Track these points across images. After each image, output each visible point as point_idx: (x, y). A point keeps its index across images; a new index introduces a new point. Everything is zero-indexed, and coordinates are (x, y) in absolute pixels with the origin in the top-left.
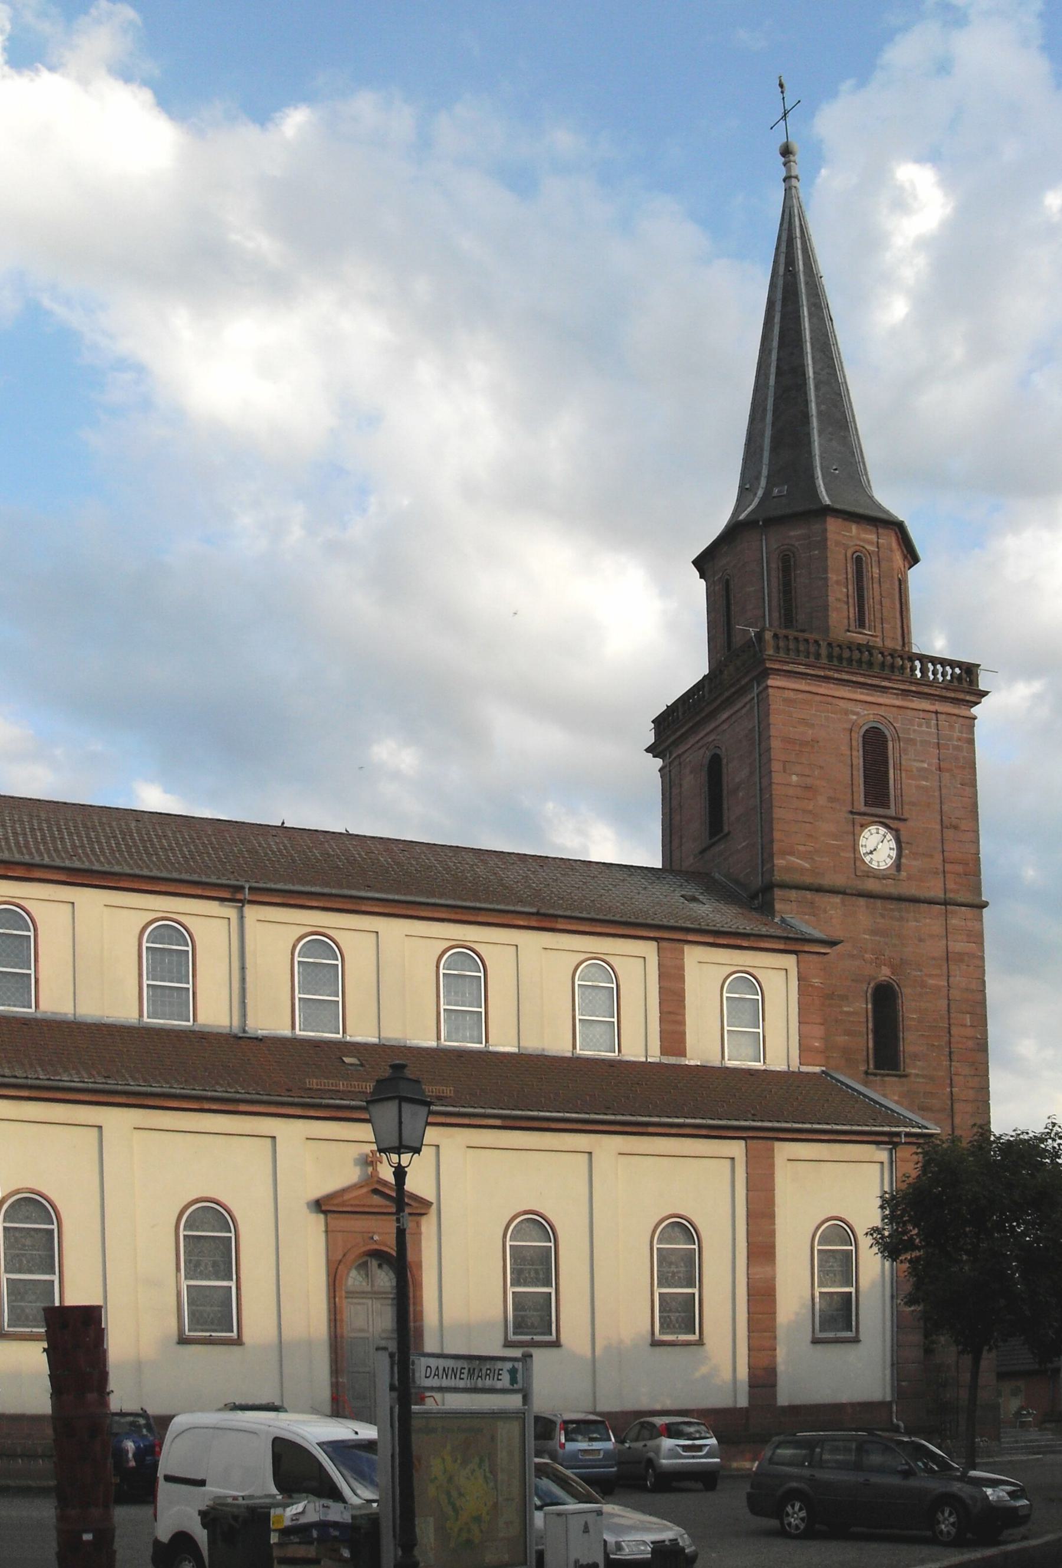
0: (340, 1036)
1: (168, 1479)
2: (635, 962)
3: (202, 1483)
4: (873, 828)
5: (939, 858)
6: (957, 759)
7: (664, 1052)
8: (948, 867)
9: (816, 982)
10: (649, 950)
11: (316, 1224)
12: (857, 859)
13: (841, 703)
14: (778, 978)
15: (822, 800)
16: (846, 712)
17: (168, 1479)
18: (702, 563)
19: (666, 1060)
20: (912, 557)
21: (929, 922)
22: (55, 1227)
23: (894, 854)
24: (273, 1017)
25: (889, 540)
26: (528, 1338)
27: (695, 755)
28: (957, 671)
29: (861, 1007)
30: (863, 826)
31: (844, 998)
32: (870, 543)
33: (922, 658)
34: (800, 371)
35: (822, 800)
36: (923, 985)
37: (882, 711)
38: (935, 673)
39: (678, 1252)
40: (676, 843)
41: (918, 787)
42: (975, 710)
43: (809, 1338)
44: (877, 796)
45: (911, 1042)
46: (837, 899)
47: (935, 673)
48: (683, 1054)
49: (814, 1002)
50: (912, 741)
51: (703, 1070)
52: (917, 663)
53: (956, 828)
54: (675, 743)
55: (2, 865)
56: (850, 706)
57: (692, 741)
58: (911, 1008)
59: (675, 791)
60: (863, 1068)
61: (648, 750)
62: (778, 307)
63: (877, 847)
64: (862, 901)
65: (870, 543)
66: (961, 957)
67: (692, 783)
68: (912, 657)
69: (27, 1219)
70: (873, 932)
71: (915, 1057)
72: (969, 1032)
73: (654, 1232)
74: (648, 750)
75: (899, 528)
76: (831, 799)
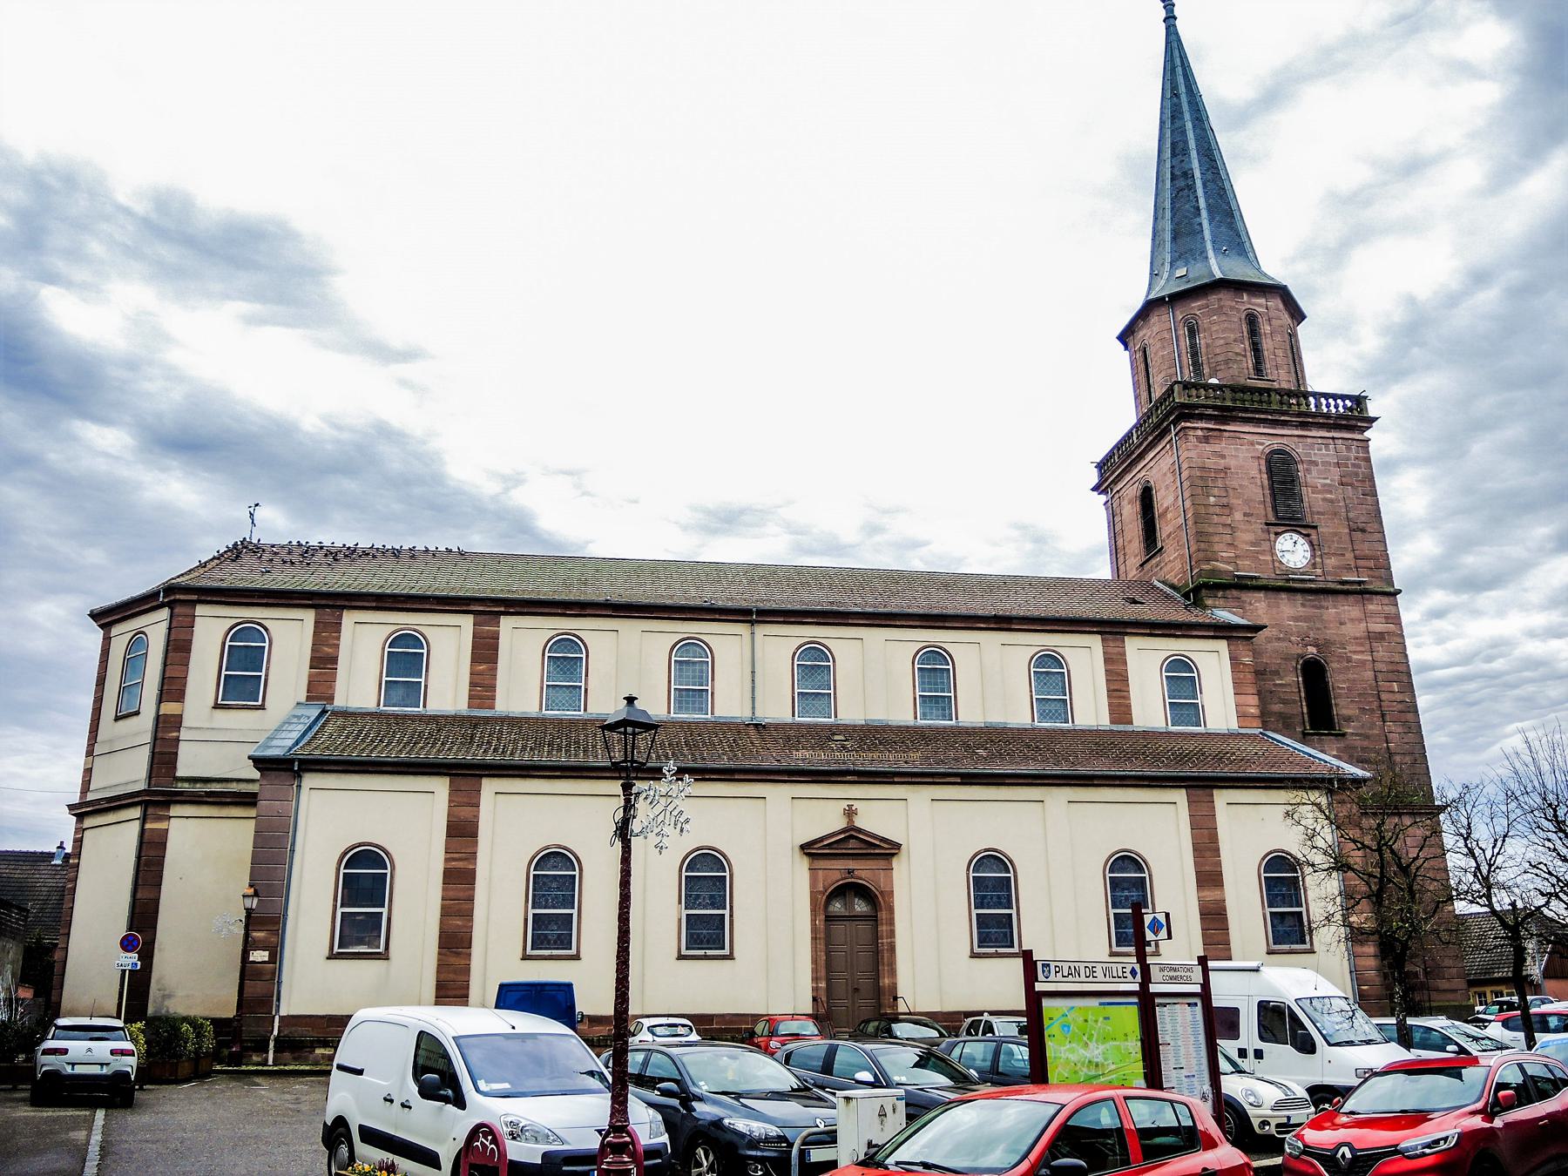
0: (953, 722)
1: (341, 1068)
2: (1084, 658)
3: (360, 1072)
4: (1287, 535)
5: (1349, 555)
6: (1357, 474)
7: (1112, 722)
8: (1361, 563)
9: (1247, 660)
10: (1095, 642)
11: (803, 864)
12: (1275, 561)
13: (1247, 436)
14: (1213, 664)
15: (1238, 516)
16: (1252, 444)
17: (341, 1068)
18: (1125, 337)
19: (1115, 727)
20: (1298, 315)
21: (1348, 609)
22: (577, 873)
23: (1308, 555)
24: (777, 707)
25: (1275, 303)
26: (701, 952)
27: (1130, 490)
28: (1348, 403)
29: (1292, 680)
30: (1277, 534)
31: (1277, 673)
32: (1260, 305)
33: (1314, 394)
34: (1188, 175)
35: (1238, 516)
36: (1349, 660)
37: (1284, 441)
38: (1328, 406)
39: (1128, 881)
40: (1121, 560)
41: (1324, 500)
42: (1367, 434)
43: (326, 952)
44: (1286, 512)
45: (1343, 707)
46: (1261, 595)
47: (1328, 406)
48: (1131, 723)
49: (1255, 678)
50: (1315, 463)
51: (1145, 734)
52: (1311, 399)
53: (1363, 531)
54: (1115, 482)
55: (1563, 666)
56: (1255, 438)
57: (1128, 477)
58: (1338, 680)
59: (1117, 519)
60: (1299, 729)
61: (1094, 489)
62: (1168, 124)
63: (1293, 552)
64: (1284, 595)
65: (1260, 305)
66: (1381, 636)
67: (1130, 511)
68: (1306, 395)
69: (555, 868)
70: (1296, 619)
71: (1348, 719)
72: (1399, 697)
73: (345, 854)
74: (1094, 489)
75: (1282, 292)
76: (1245, 515)
